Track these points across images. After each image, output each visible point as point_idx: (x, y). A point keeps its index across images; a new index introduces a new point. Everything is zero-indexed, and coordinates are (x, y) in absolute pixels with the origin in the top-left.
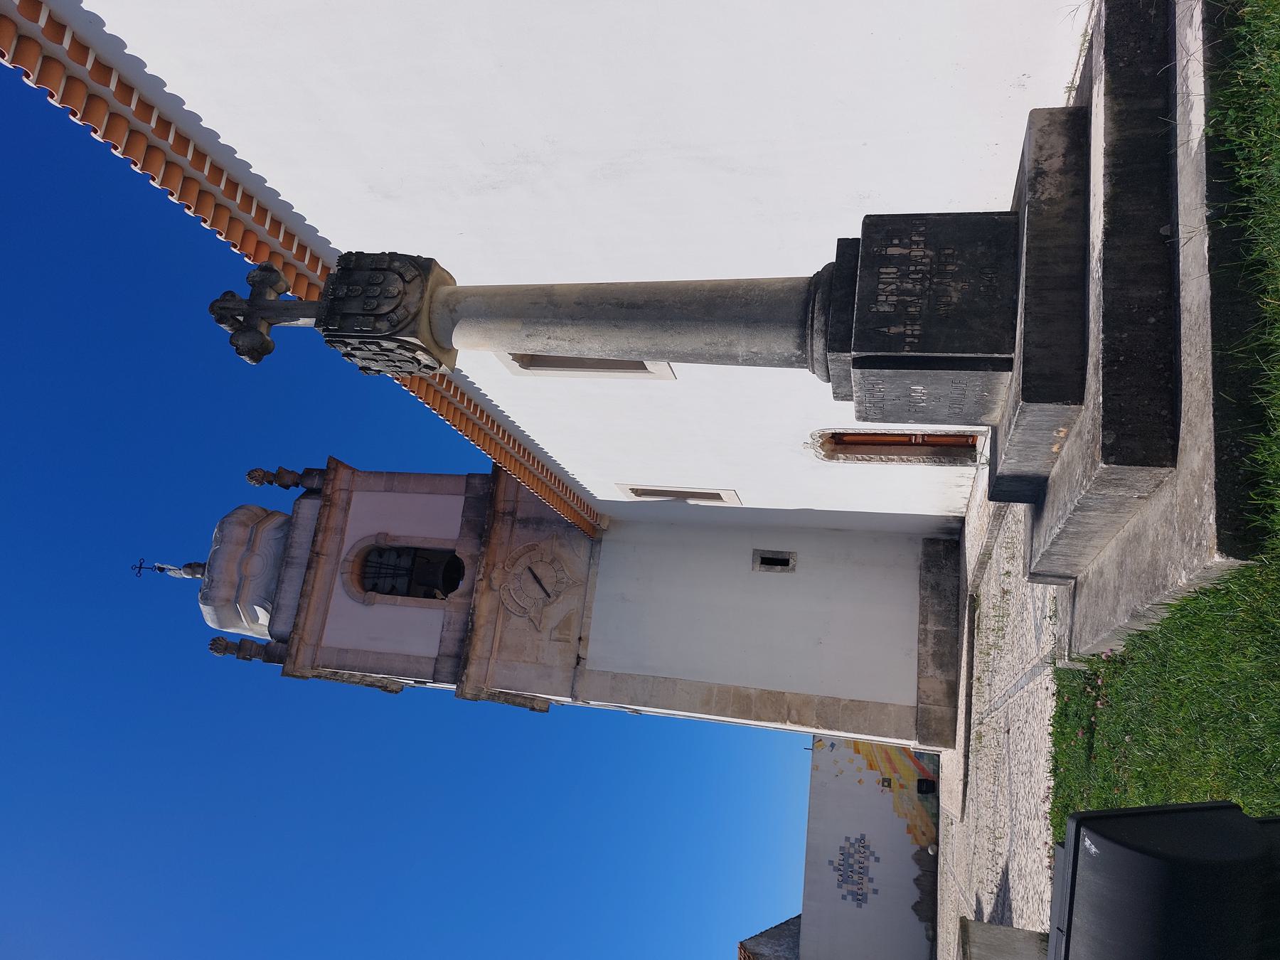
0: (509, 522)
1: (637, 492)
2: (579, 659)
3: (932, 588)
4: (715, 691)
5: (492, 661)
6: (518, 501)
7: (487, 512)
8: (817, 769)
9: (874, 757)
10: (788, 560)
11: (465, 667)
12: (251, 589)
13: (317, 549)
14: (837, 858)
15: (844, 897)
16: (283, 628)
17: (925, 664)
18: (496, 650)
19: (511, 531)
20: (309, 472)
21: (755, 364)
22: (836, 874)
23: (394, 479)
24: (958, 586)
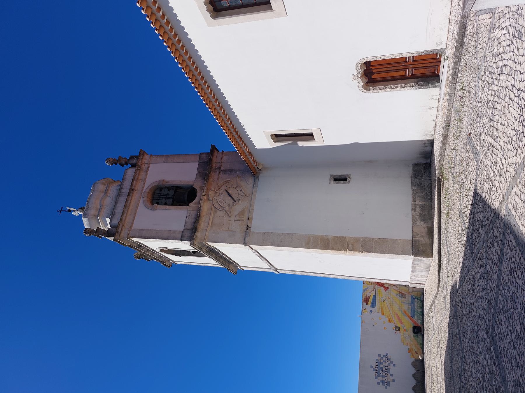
0: (218, 172)
1: (277, 137)
2: (248, 227)
3: (418, 185)
5: (208, 230)
6: (222, 163)
7: (208, 167)
8: (364, 323)
9: (391, 317)
10: (347, 178)
11: (195, 232)
13: (133, 187)
14: (375, 365)
15: (378, 383)
16: (115, 222)
17: (416, 220)
18: (210, 226)
19: (219, 175)
20: (132, 157)
22: (374, 372)
24: (431, 184)
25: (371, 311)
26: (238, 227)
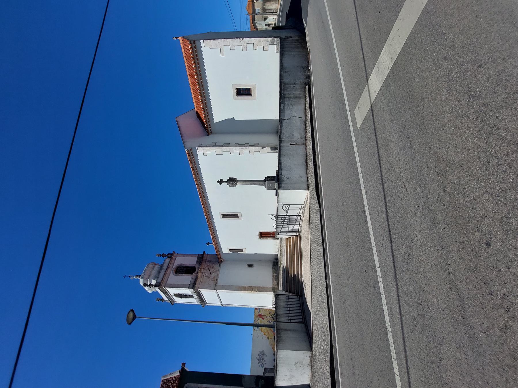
1: (231, 250)
2: (216, 283)
4: (240, 287)
11: (195, 285)
12: (152, 276)
13: (169, 266)
14: (258, 356)
15: (259, 366)
16: (159, 281)
19: (205, 263)
20: (169, 254)
21: (280, 98)
22: (258, 360)
23: (184, 255)
25: (257, 330)
26: (212, 283)
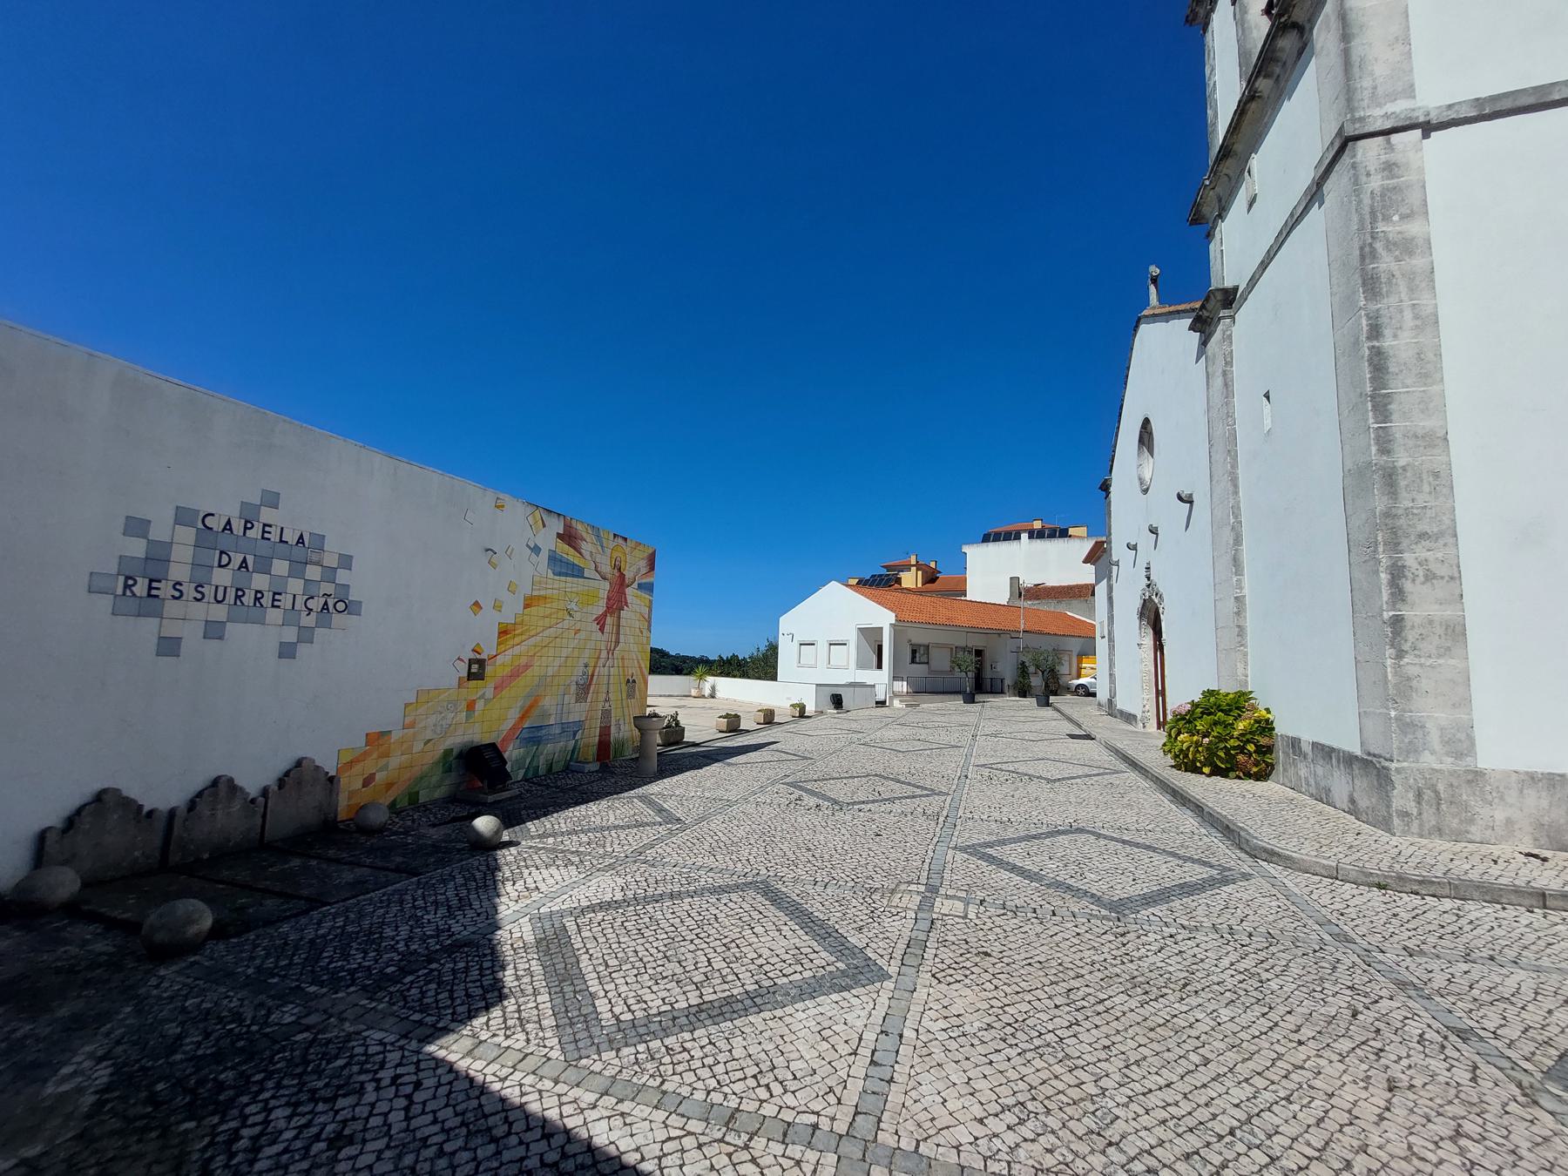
14: (287, 520)
